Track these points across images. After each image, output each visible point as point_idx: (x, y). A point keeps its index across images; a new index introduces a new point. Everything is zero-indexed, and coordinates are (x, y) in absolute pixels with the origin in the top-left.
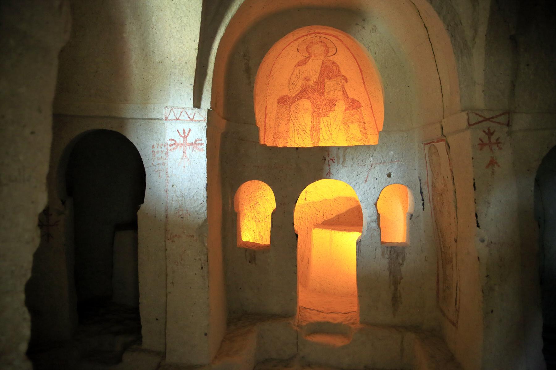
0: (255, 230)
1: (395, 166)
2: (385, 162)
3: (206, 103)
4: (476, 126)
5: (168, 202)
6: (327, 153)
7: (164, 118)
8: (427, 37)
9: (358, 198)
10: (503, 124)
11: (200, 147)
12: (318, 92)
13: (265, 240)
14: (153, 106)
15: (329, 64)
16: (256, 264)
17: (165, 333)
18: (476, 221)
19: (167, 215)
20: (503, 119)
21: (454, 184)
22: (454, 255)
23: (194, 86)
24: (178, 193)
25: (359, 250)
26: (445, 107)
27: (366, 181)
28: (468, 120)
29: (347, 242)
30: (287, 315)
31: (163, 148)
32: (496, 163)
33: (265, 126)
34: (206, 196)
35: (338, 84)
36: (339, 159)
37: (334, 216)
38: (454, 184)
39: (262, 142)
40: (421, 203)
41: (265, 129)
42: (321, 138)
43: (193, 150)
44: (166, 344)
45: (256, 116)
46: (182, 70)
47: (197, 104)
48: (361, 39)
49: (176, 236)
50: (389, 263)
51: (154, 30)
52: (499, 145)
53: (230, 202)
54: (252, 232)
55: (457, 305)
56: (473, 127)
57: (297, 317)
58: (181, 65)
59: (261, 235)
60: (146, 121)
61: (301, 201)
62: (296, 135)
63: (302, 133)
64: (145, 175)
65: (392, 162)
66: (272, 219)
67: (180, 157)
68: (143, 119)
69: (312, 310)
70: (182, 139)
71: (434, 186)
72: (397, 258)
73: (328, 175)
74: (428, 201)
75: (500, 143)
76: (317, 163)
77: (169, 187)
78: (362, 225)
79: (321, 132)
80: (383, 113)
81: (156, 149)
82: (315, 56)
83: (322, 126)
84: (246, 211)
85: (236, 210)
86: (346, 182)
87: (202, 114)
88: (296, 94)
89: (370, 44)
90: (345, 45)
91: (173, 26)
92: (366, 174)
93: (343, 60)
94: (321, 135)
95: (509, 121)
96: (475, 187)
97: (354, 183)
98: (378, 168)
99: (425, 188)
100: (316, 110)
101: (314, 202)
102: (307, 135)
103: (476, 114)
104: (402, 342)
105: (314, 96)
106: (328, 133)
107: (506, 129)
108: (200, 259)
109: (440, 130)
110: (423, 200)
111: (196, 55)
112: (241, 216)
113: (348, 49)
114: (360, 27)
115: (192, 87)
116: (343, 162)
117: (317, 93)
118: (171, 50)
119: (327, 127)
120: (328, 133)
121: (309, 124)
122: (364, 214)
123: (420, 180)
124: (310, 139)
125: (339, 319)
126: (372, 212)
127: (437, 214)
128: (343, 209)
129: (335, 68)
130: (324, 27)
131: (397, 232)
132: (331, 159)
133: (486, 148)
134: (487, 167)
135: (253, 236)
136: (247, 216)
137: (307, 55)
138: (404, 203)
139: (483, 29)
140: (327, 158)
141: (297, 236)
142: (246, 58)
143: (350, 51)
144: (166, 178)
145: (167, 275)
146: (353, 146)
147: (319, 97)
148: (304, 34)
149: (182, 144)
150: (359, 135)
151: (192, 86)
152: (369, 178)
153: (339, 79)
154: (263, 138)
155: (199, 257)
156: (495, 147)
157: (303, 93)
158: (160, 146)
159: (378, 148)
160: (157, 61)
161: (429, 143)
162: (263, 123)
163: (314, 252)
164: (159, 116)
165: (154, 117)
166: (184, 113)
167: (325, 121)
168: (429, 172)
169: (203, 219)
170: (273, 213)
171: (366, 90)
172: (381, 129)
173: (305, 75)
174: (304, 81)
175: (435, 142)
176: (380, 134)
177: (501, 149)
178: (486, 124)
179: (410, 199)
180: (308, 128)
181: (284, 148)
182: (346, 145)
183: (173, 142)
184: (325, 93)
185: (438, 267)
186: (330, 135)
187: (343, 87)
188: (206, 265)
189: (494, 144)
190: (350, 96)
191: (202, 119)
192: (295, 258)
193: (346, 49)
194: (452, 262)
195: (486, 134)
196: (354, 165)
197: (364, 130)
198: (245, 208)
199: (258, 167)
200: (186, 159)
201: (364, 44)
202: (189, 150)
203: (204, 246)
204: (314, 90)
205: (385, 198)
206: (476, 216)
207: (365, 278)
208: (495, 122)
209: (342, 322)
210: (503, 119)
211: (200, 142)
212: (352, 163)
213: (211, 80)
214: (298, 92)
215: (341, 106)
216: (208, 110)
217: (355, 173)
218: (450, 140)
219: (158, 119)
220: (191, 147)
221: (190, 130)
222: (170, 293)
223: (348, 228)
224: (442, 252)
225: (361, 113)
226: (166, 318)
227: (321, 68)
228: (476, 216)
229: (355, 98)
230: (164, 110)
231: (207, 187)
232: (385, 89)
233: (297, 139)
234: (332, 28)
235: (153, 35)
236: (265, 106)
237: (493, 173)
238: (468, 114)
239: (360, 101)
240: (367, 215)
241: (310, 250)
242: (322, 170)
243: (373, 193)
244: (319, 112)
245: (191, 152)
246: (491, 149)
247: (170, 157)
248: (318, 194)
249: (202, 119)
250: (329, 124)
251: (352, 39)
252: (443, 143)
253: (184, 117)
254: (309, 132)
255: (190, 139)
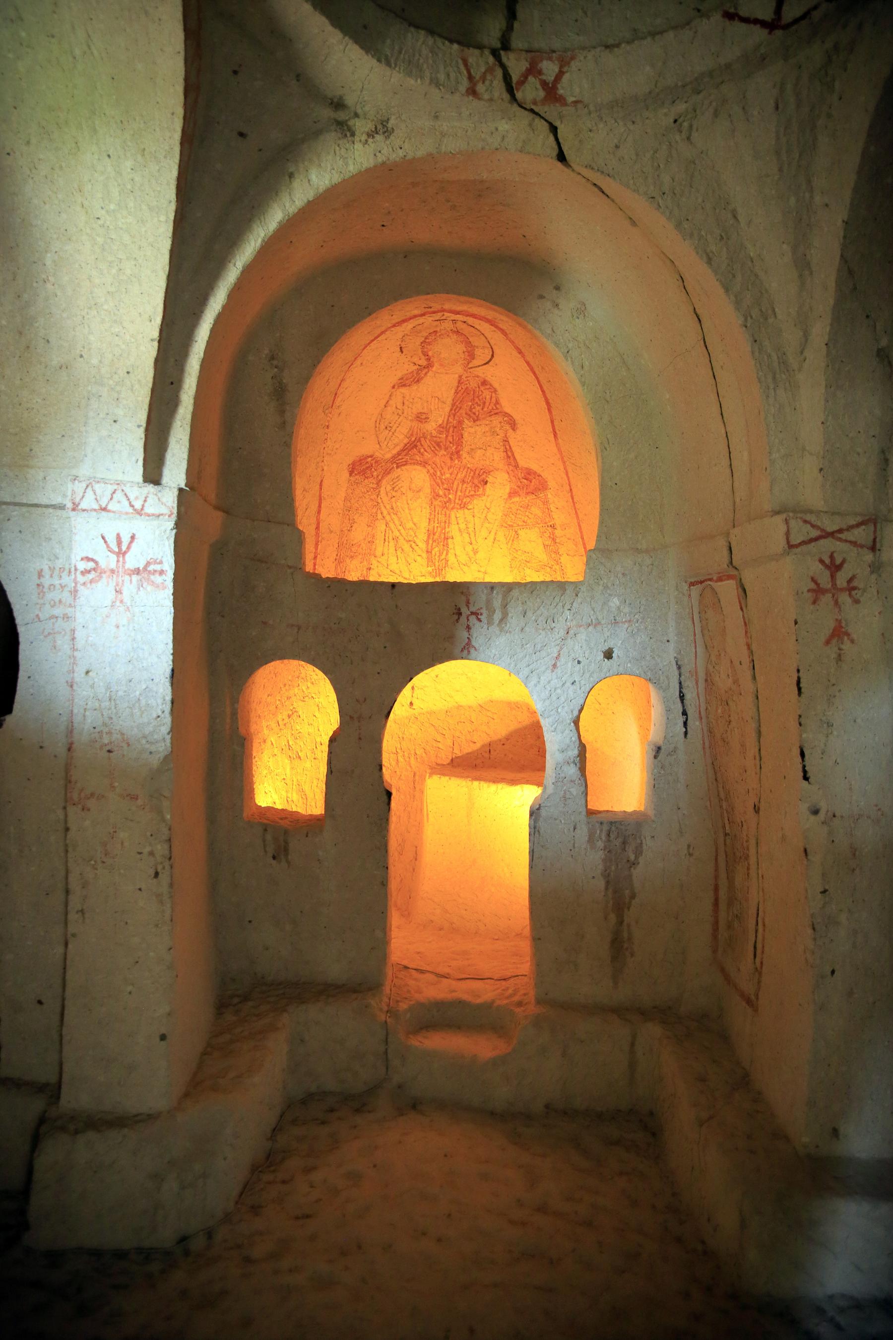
0: (287, 776)
1: (622, 631)
2: (599, 623)
3: (176, 472)
4: (804, 548)
5: (75, 711)
6: (463, 598)
7: (69, 505)
8: (700, 337)
9: (538, 707)
10: (862, 546)
11: (158, 579)
12: (446, 449)
13: (317, 807)
14: (41, 474)
15: (473, 384)
16: (288, 862)
17: (61, 1036)
18: (800, 766)
19: (72, 744)
20: (861, 534)
21: (754, 678)
22: (753, 842)
23: (147, 430)
24: (101, 690)
25: (534, 830)
26: (738, 500)
27: (555, 666)
28: (788, 534)
29: (507, 809)
30: (361, 987)
31: (67, 580)
32: (848, 634)
33: (318, 528)
34: (169, 698)
35: (495, 433)
36: (492, 612)
37: (478, 745)
38: (754, 678)
39: (309, 568)
40: (681, 719)
41: (317, 535)
42: (451, 558)
43: (140, 586)
44: (61, 1065)
45: (297, 504)
46: (118, 388)
47: (153, 474)
48: (549, 331)
49: (92, 795)
50: (604, 861)
51: (49, 286)
52: (854, 593)
53: (228, 710)
54: (280, 784)
55: (758, 960)
56: (799, 550)
57: (387, 989)
58: (116, 376)
59: (301, 792)
60: (24, 509)
61: (399, 710)
62: (392, 550)
63: (406, 547)
64: (17, 643)
65: (616, 622)
66: (330, 753)
67: (108, 602)
68: (15, 504)
69: (422, 972)
70: (114, 558)
71: (709, 681)
72: (624, 850)
73: (465, 651)
74: (697, 715)
75: (854, 588)
76: (441, 620)
77: (79, 676)
78: (543, 768)
79: (451, 546)
80: (598, 505)
81: (46, 581)
82: (441, 365)
83: (453, 530)
84: (266, 731)
85: (242, 731)
86: (507, 667)
87: (164, 500)
88: (395, 452)
89: (570, 345)
90: (512, 342)
91: (97, 281)
92: (555, 651)
93: (507, 377)
94: (451, 552)
95: (874, 540)
96: (799, 689)
97: (526, 671)
98: (582, 636)
99: (689, 684)
100: (441, 493)
101: (431, 713)
102: (420, 552)
103: (805, 522)
104: (633, 1044)
105: (437, 460)
106: (469, 548)
107: (869, 557)
108: (151, 854)
109: (726, 553)
110: (684, 713)
111: (154, 353)
112: (255, 745)
113: (520, 352)
114: (548, 305)
115: (141, 433)
116: (501, 620)
117: (443, 452)
118: (92, 338)
119: (466, 536)
120: (469, 548)
121: (424, 525)
122: (548, 746)
123: (679, 668)
124: (425, 562)
125: (486, 993)
126: (567, 741)
127: (715, 745)
128: (500, 729)
129: (487, 394)
130: (462, 298)
131: (626, 787)
132: (472, 613)
133: (827, 598)
134: (828, 642)
135: (284, 794)
136: (268, 744)
137: (423, 362)
138: (643, 719)
139: (820, 331)
140: (465, 611)
141: (389, 794)
142: (275, 362)
143: (523, 356)
144: (69, 652)
145: (67, 892)
146: (526, 584)
147: (448, 461)
148: (416, 312)
149: (113, 571)
150: (540, 554)
151: (142, 430)
152: (562, 660)
153: (496, 421)
154: (312, 555)
155: (147, 850)
156: (844, 598)
157: (410, 451)
158: (57, 572)
159: (583, 588)
160: (54, 363)
161: (701, 582)
162: (314, 520)
163: (429, 831)
164: (57, 500)
165: (44, 501)
166: (119, 495)
167: (461, 521)
168: (700, 650)
169: (162, 755)
170: (332, 740)
171: (559, 450)
172: (591, 545)
173: (418, 407)
174: (415, 424)
175: (714, 584)
176: (590, 555)
177: (857, 602)
178: (827, 545)
179: (656, 712)
180: (422, 536)
181: (364, 584)
182: (509, 579)
183: (91, 565)
184: (464, 454)
185: (716, 870)
186: (471, 554)
187: (506, 441)
188: (167, 867)
189: (842, 590)
190: (522, 463)
191: (165, 511)
192: (383, 847)
193: (515, 353)
194: (747, 857)
195: (827, 567)
196: (527, 629)
197: (552, 544)
198: (264, 724)
199: (299, 628)
200: (122, 609)
201: (557, 345)
202: (130, 586)
203: (163, 820)
204: (438, 444)
205: (597, 706)
206: (802, 755)
207: (549, 897)
208: (846, 541)
209: (493, 1002)
210: (861, 534)
211: (158, 567)
212: (522, 624)
213: (189, 417)
214: (398, 449)
215: (500, 486)
216: (181, 490)
217: (529, 648)
218: (749, 576)
219: (54, 507)
220: (135, 578)
221: (133, 538)
222: (74, 935)
223: (510, 775)
224: (726, 835)
225: (546, 502)
226: (63, 999)
227: (456, 392)
228: (802, 755)
229: (534, 467)
230: (70, 485)
231: (172, 676)
232: (603, 448)
233: (393, 560)
234: (482, 302)
235: (47, 299)
236: (319, 480)
237: (839, 658)
238: (787, 521)
239: (545, 475)
240: (557, 747)
241: (419, 828)
242: (451, 638)
243: (571, 693)
244: (447, 498)
245: (135, 591)
246: (836, 602)
247: (82, 600)
248: (441, 695)
249: (165, 511)
250: (471, 526)
251: (529, 331)
252: (732, 583)
253: (119, 505)
254: (423, 545)
255: (134, 560)
